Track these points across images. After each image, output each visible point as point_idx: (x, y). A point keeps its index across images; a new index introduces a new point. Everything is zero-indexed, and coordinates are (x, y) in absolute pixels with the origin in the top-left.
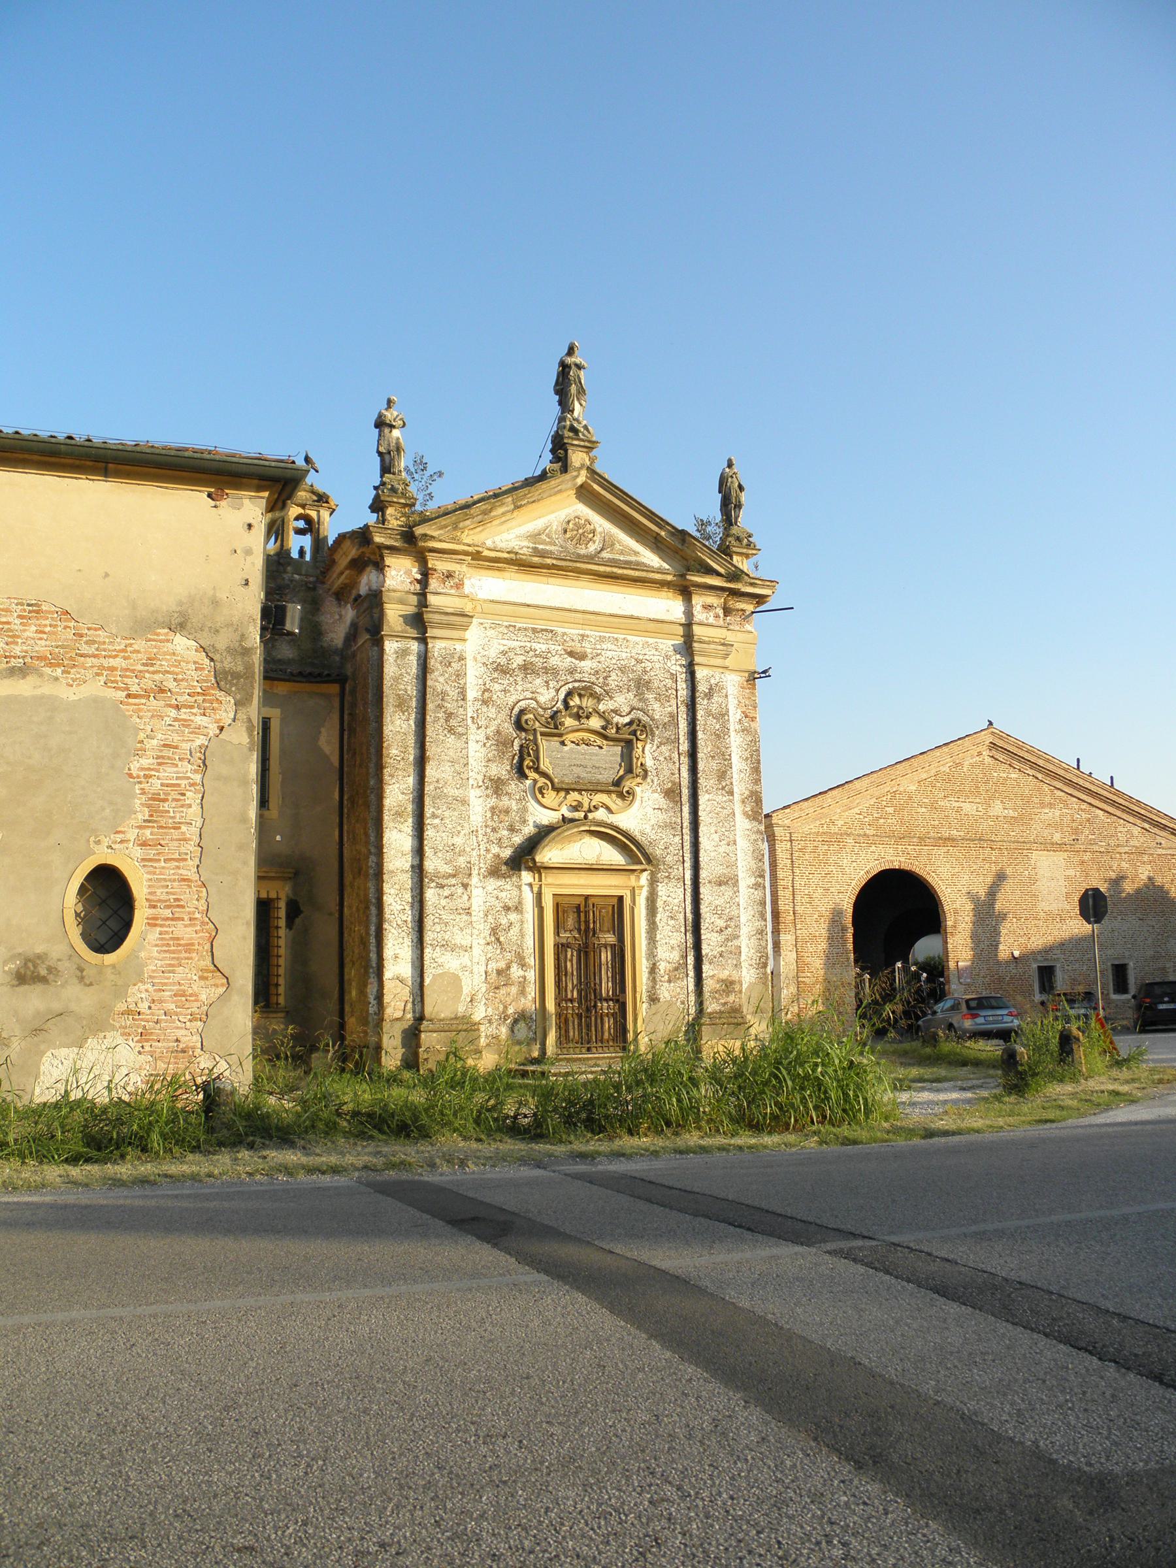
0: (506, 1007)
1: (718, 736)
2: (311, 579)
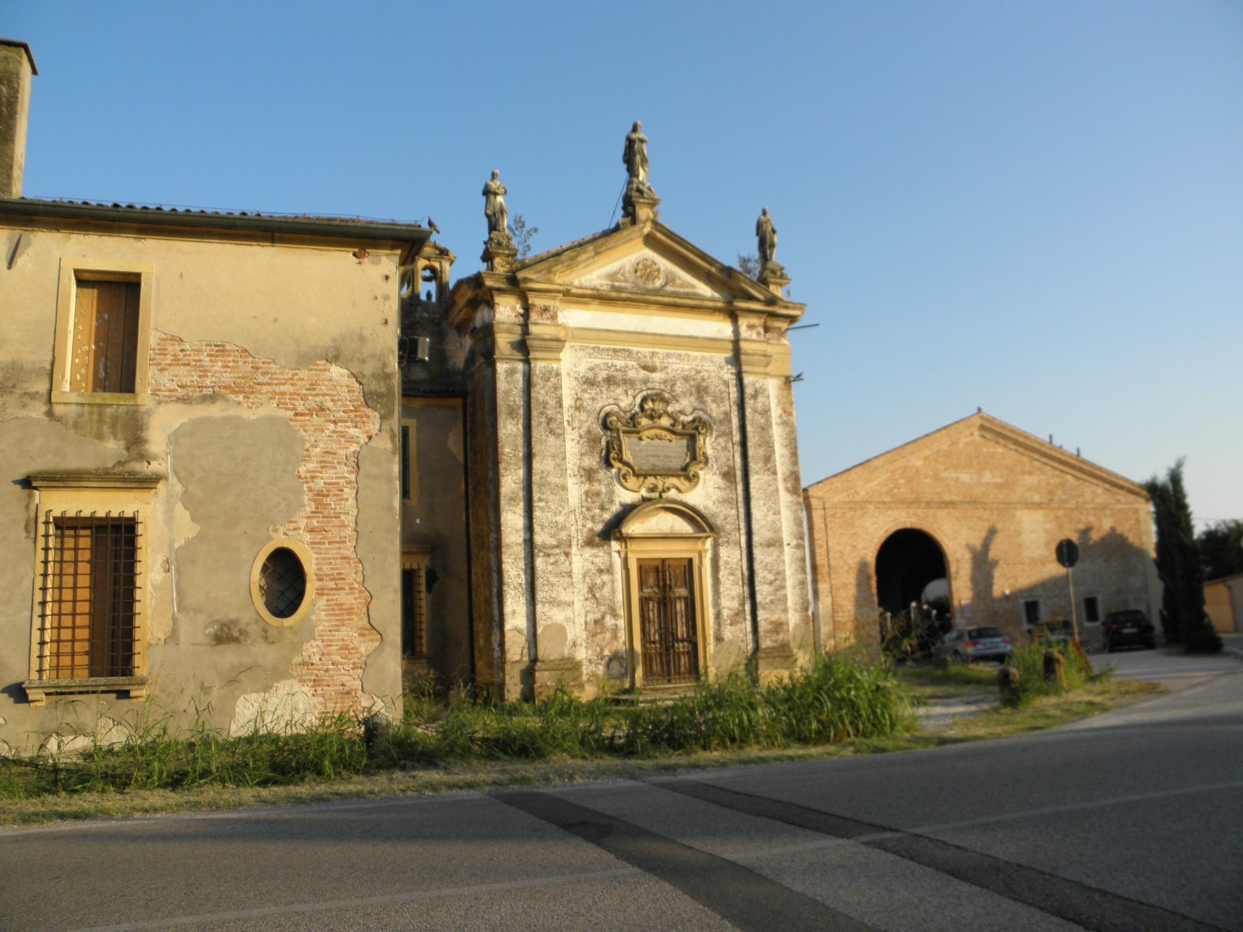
0: (602, 650)
1: (763, 429)
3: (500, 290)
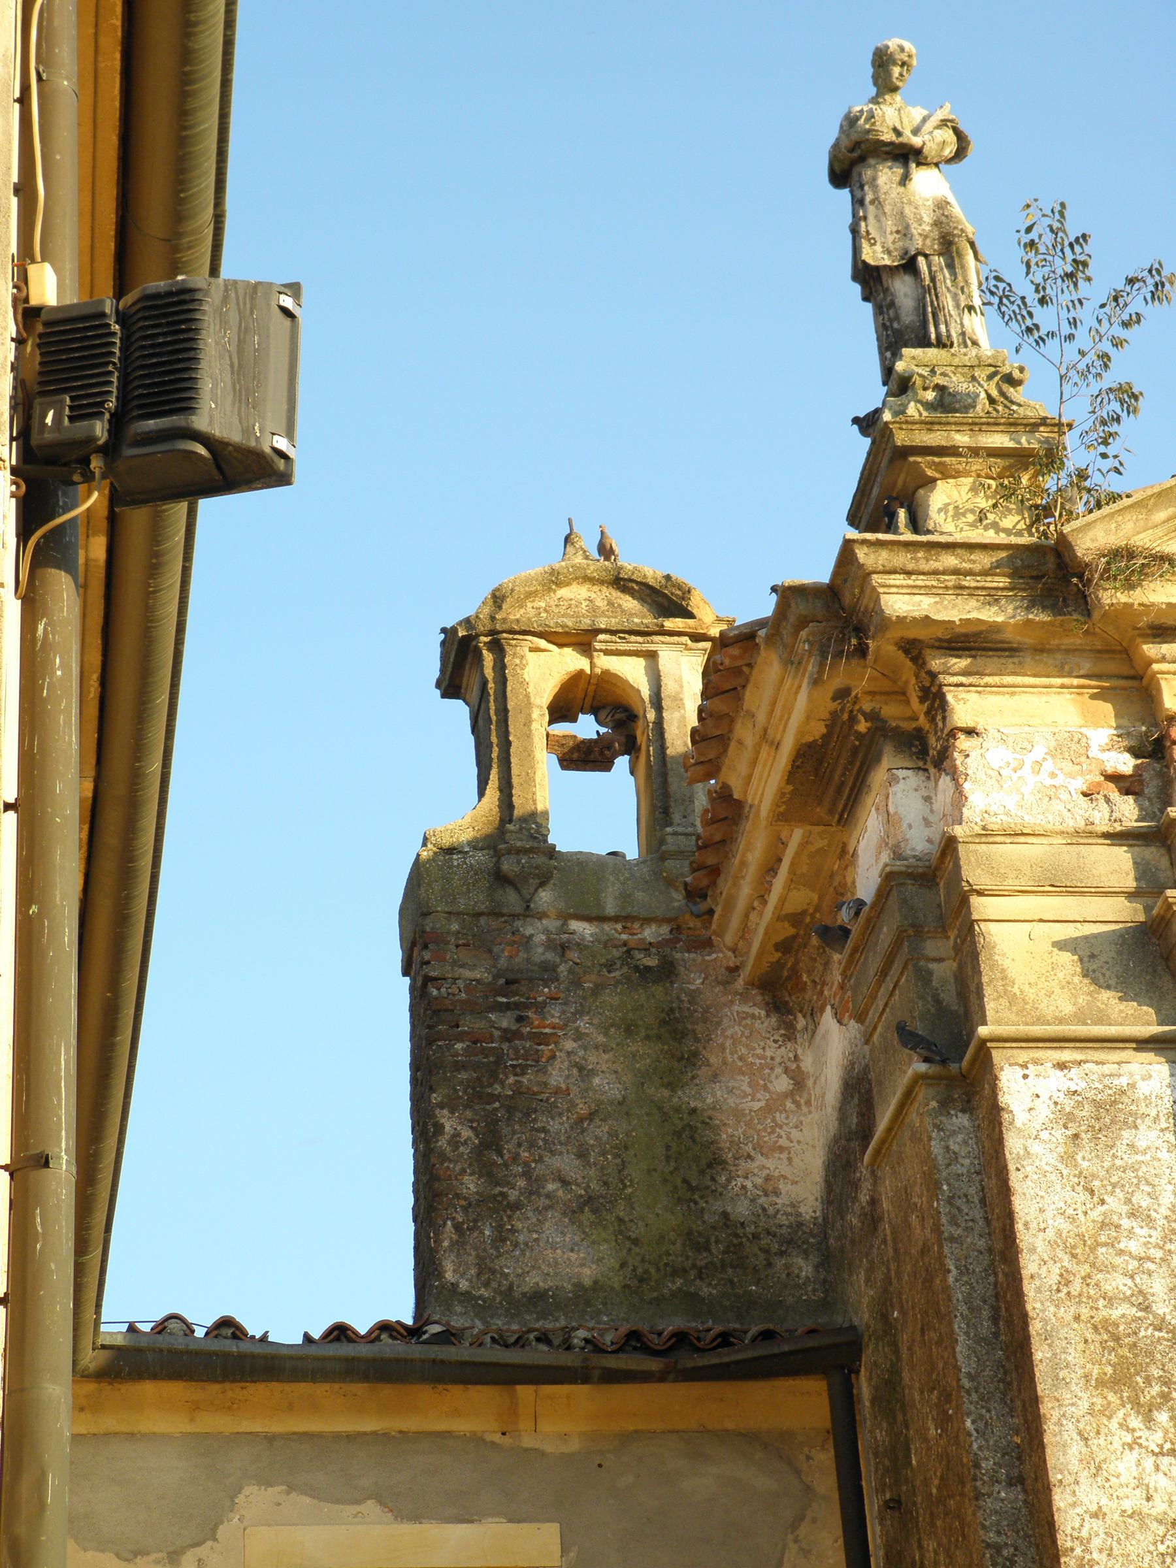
2: (649, 933)
3: (972, 643)
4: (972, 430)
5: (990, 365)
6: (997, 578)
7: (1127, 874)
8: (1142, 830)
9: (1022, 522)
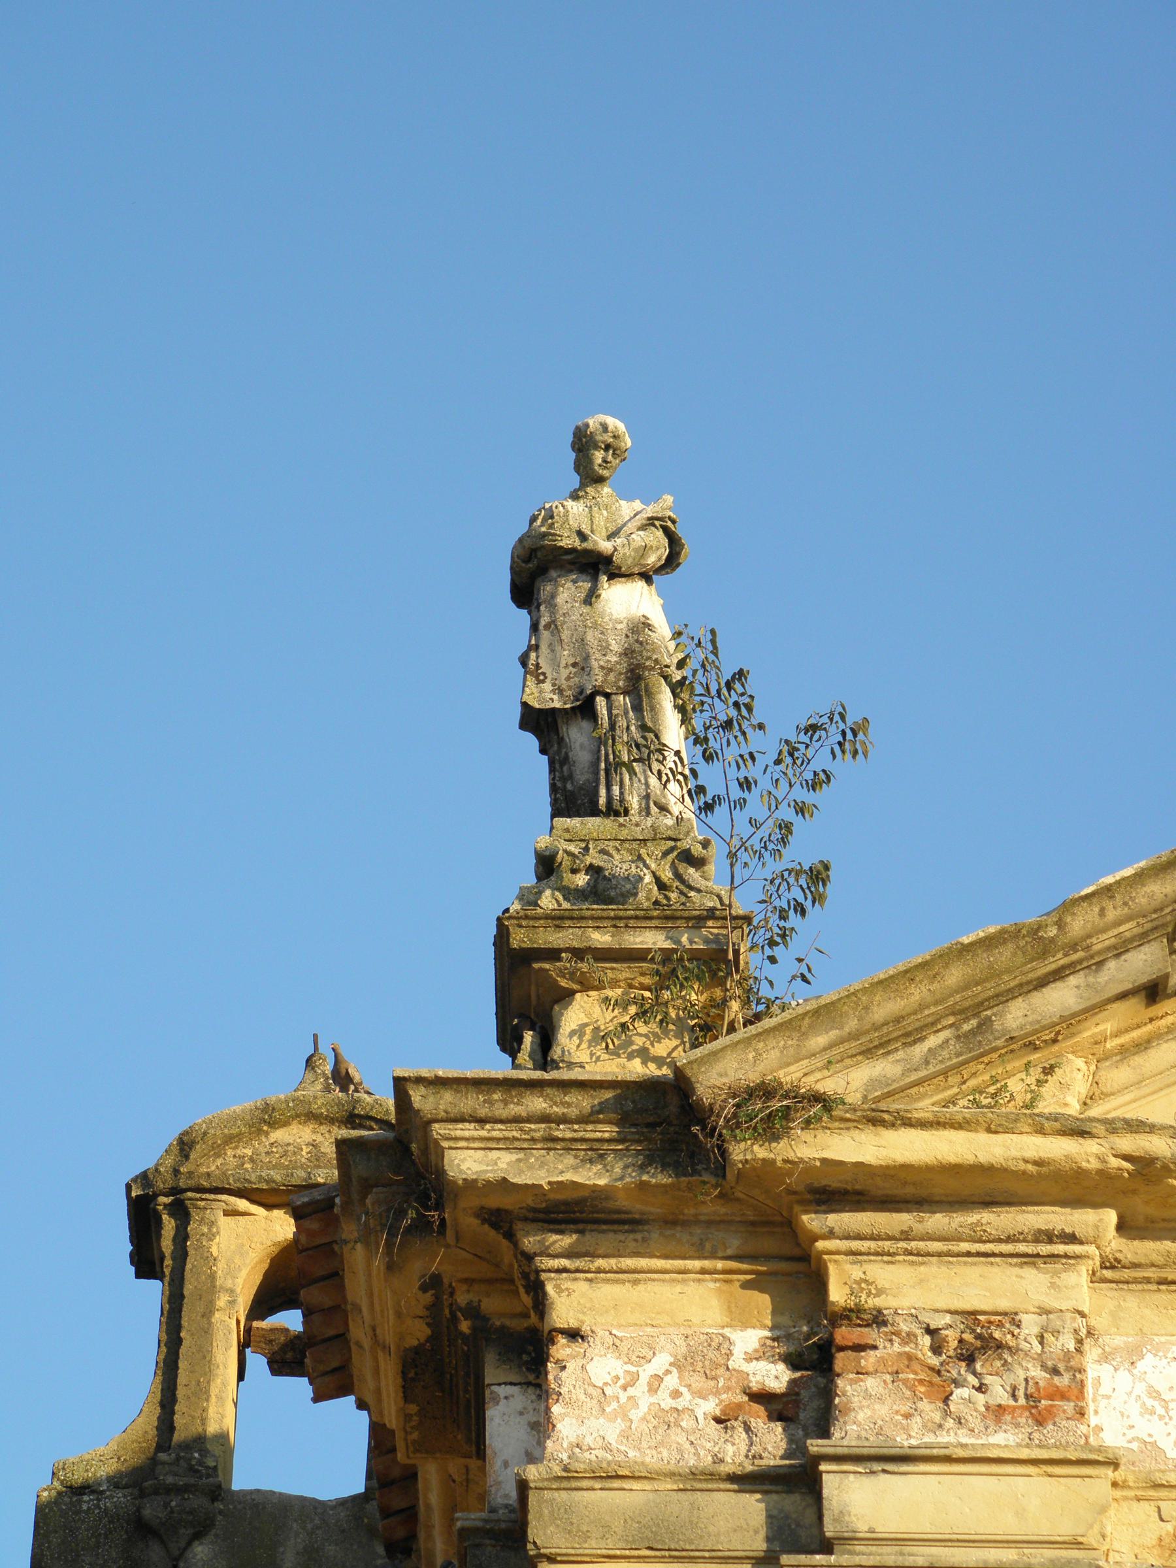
4: (615, 926)
5: (670, 839)
6: (600, 1127)
7: (756, 1532)
8: (781, 1471)
9: (680, 1049)
